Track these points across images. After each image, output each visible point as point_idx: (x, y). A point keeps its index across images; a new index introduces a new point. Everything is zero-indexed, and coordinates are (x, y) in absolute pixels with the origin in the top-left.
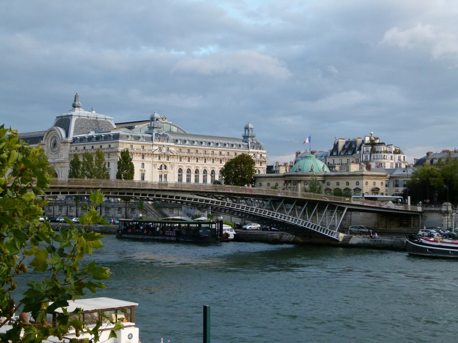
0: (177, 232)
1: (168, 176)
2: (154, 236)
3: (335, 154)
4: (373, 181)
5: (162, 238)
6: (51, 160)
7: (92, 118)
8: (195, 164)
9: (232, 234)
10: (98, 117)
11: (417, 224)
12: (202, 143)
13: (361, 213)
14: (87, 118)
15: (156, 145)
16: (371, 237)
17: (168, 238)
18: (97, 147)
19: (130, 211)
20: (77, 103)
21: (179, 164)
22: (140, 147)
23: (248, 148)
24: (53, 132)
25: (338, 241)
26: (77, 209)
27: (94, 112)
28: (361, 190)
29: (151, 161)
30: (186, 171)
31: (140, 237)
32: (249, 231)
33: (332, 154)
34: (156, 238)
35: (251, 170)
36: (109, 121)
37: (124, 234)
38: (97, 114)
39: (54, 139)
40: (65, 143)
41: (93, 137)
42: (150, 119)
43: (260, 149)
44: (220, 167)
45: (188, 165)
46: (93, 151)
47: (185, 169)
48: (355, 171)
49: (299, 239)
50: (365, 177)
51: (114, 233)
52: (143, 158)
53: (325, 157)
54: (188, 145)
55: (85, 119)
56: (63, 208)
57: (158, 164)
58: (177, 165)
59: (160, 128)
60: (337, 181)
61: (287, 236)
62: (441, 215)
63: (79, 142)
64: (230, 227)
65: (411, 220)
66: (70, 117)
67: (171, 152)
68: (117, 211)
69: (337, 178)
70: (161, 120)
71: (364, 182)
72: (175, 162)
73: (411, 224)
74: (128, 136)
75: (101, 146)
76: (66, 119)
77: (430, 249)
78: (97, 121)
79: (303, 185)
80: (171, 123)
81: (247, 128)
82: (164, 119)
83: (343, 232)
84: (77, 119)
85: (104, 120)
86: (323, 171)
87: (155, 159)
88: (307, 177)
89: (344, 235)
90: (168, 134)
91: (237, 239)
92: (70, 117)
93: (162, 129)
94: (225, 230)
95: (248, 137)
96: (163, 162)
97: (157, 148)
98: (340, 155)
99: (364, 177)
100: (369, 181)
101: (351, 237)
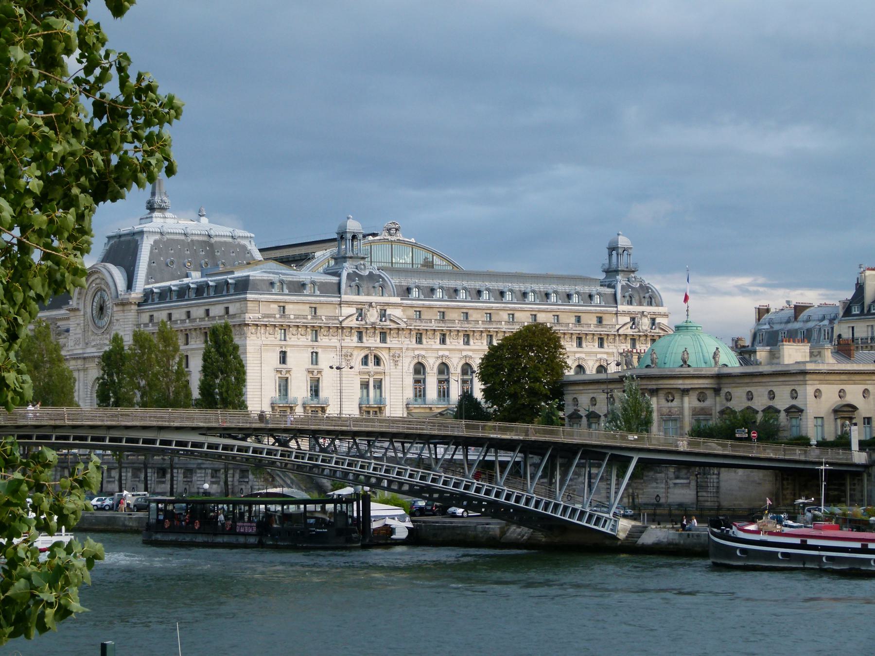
0: (260, 525)
1: (386, 385)
2: (215, 535)
3: (856, 311)
4: (837, 388)
5: (232, 539)
6: (94, 350)
7: (196, 238)
8: (461, 350)
10: (212, 233)
11: (858, 496)
12: (479, 292)
13: (740, 471)
14: (183, 237)
15: (349, 304)
16: (683, 526)
17: (242, 540)
18: (162, 316)
19: (237, 476)
20: (157, 199)
21: (417, 353)
22: (305, 310)
23: (616, 302)
24: (96, 276)
25: (614, 538)
26: (120, 476)
27: (204, 220)
28: (801, 411)
29: (338, 345)
30: (435, 370)
31: (188, 539)
32: (461, 520)
33: (848, 312)
34: (219, 539)
35: (555, 366)
36: (243, 242)
37: (157, 532)
38: (212, 226)
39: (99, 293)
40: (124, 304)
41: (189, 288)
42: (335, 236)
43: (650, 304)
45: (441, 353)
46: (151, 328)
47: (432, 365)
48: (797, 363)
49: (541, 537)
51: (136, 532)
53: (832, 321)
54: (439, 300)
55: (177, 241)
57: (355, 353)
58: (411, 353)
59: (363, 258)
60: (748, 389)
61: (516, 532)
63: (157, 300)
64: (402, 512)
65: (844, 485)
66: (137, 238)
69: (747, 380)
70: (385, 235)
71: (810, 389)
73: (845, 496)
74: (272, 284)
75: (170, 315)
76: (129, 242)
77: (743, 551)
78: (211, 245)
79: (696, 404)
80: (413, 240)
81: (613, 248)
82: (393, 231)
84: (155, 242)
85: (230, 240)
86: (716, 363)
87: (348, 339)
89: (633, 523)
90: (383, 274)
91: (415, 539)
92: (137, 238)
93: (367, 262)
95: (617, 272)
97: (628, 319)
98: (869, 313)
99: (808, 377)
100: (823, 388)
101: (646, 527)
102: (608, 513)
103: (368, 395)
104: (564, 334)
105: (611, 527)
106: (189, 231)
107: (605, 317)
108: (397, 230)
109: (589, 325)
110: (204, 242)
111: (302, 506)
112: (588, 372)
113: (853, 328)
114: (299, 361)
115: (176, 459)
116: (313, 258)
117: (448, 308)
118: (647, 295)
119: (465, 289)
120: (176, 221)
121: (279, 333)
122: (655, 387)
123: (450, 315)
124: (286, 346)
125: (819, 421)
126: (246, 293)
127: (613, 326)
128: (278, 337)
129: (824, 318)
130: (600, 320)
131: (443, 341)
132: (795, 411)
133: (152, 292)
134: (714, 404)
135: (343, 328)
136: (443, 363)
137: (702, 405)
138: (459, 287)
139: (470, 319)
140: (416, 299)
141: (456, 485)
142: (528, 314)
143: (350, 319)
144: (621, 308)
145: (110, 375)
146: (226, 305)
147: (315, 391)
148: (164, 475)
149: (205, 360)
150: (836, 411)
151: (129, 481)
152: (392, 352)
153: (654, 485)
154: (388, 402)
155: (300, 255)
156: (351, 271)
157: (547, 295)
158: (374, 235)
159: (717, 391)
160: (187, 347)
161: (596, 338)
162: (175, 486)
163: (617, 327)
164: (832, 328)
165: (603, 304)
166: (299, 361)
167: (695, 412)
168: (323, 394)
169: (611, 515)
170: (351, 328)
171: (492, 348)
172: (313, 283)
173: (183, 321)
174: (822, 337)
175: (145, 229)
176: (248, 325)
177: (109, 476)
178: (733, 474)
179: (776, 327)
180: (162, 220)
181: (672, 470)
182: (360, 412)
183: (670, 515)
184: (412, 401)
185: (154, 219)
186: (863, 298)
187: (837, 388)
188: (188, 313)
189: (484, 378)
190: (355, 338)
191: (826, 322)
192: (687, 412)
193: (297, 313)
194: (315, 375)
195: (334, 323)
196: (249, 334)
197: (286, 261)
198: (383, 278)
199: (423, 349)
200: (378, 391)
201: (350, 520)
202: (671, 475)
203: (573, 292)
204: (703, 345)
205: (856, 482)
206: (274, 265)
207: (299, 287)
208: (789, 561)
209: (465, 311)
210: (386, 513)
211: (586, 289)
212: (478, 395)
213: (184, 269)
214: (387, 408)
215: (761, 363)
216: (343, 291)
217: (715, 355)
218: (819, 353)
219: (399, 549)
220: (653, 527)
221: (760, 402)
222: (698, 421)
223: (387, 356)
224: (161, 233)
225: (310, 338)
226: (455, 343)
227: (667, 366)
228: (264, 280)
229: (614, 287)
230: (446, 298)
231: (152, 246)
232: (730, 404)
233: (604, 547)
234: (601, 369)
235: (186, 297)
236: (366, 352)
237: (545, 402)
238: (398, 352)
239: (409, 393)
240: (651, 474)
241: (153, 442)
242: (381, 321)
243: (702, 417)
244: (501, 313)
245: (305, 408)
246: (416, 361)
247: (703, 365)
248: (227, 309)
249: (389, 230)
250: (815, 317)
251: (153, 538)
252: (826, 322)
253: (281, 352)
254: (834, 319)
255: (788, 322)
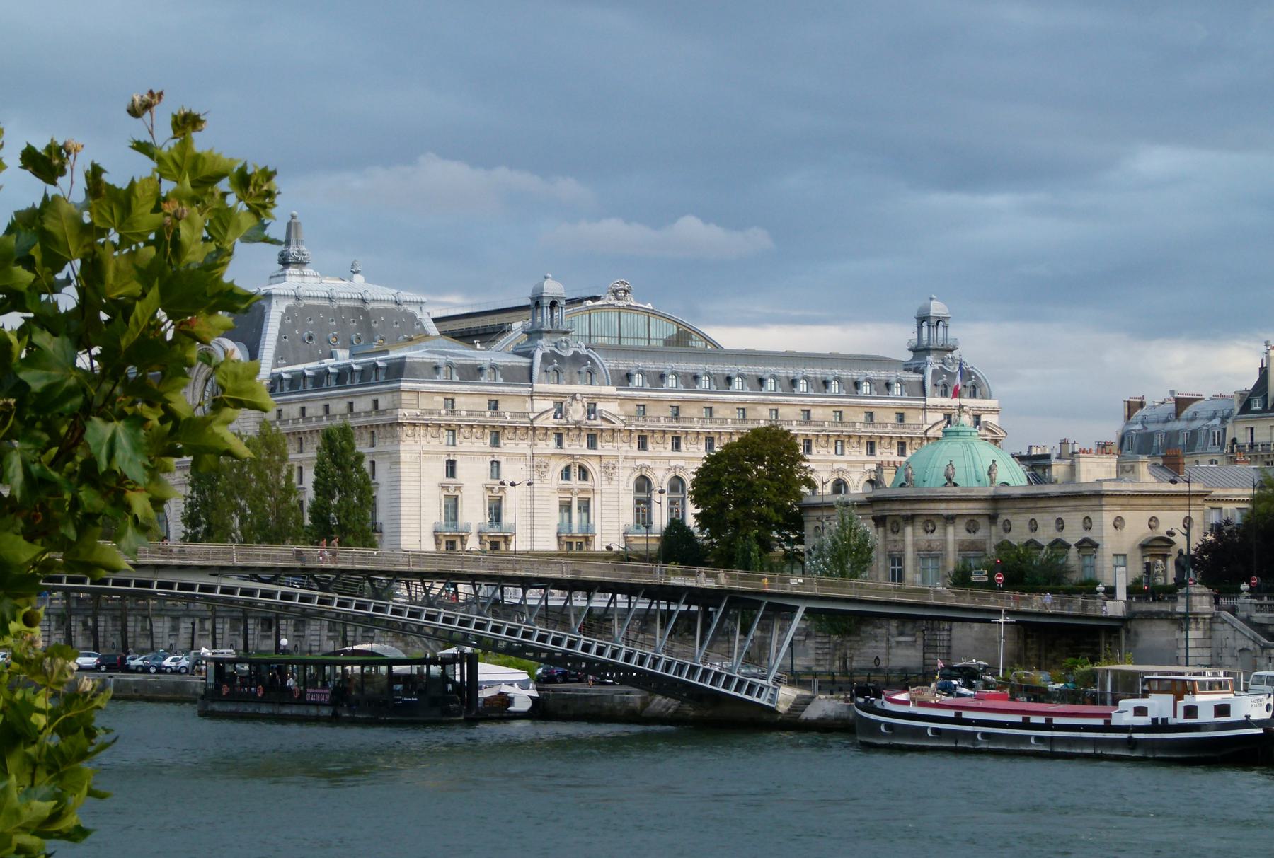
1: (595, 506)
3: (1256, 406)
4: (1146, 515)
9: (522, 699)
10: (367, 296)
12: (729, 380)
13: (976, 626)
14: (327, 303)
15: (545, 395)
17: (313, 711)
20: (293, 250)
21: (639, 462)
25: (773, 711)
26: (214, 628)
27: (359, 279)
28: (1096, 546)
29: (528, 451)
31: (250, 710)
33: (1246, 408)
34: (287, 710)
36: (410, 309)
37: (213, 701)
38: (370, 286)
41: (327, 373)
42: (529, 302)
43: (973, 395)
44: (868, 467)
45: (673, 463)
47: (661, 478)
49: (690, 711)
50: (1114, 500)
51: (193, 702)
52: (495, 443)
53: (1224, 420)
54: (671, 391)
55: (318, 308)
56: (182, 625)
57: (552, 463)
58: (631, 464)
60: (1031, 516)
61: (660, 703)
62: (1174, 627)
63: (286, 389)
64: (525, 677)
65: (1098, 644)
66: (264, 303)
67: (603, 418)
68: (325, 632)
69: (1030, 505)
70: (609, 299)
71: (1108, 518)
72: (622, 454)
74: (436, 368)
77: (888, 726)
78: (366, 314)
79: (964, 535)
80: (649, 306)
82: (621, 294)
83: (791, 683)
84: (288, 309)
85: (393, 306)
86: (992, 481)
87: (541, 444)
88: (932, 506)
91: (539, 711)
92: (264, 303)
94: (491, 684)
96: (572, 456)
97: (940, 417)
99: (1105, 500)
100: (1127, 515)
101: (812, 698)
102: (765, 678)
103: (570, 521)
104: (849, 437)
105: (768, 696)
106: (335, 294)
107: (908, 413)
108: (626, 292)
109: (885, 425)
110: (357, 309)
111: (339, 669)
112: (852, 490)
113: (1252, 429)
114: (473, 475)
115: (191, 606)
116: (510, 330)
117: (684, 401)
118: (969, 383)
119: (708, 374)
120: (318, 280)
121: (445, 436)
122: (909, 513)
123: (686, 411)
124: (455, 453)
125: (1121, 560)
126: (399, 381)
127: (919, 426)
128: (445, 440)
129: (1213, 418)
130: (901, 418)
131: (677, 447)
132: (1088, 546)
133: (280, 378)
134: (989, 536)
135: (535, 429)
136: (677, 477)
137: (972, 537)
138: (700, 373)
139: (715, 416)
140: (639, 389)
141: (557, 641)
142: (798, 409)
143: (545, 416)
144: (931, 401)
145: (201, 492)
146: (375, 397)
147: (496, 513)
148: (270, 629)
149: (317, 474)
150: (1143, 547)
151: (226, 636)
152: (604, 461)
153: (873, 643)
154: (597, 530)
155: (493, 327)
156: (547, 350)
157: (826, 383)
158: (596, 298)
159: (993, 518)
160: (301, 456)
161: (895, 442)
162: (250, 642)
163: (926, 427)
164: (1225, 430)
165: (905, 395)
166: (473, 475)
167: (963, 547)
168: (507, 519)
169: (770, 681)
170: (546, 428)
171: (710, 459)
172: (494, 368)
173: (319, 418)
174: (1211, 442)
175: (274, 292)
176: (402, 424)
177: (203, 629)
178: (968, 630)
179: (1151, 428)
180: (299, 279)
181: (894, 624)
182: (559, 544)
183: (833, 682)
184: (633, 529)
185: (288, 278)
186: (1266, 389)
187: (1146, 515)
188: (327, 407)
189: (697, 501)
190: (552, 442)
191: (1217, 421)
192: (951, 547)
193: (472, 408)
194: (496, 493)
195: (524, 422)
196: (403, 437)
197: (465, 337)
198: (593, 362)
199: (647, 458)
200: (585, 515)
201: (450, 687)
202: (893, 630)
203: (862, 379)
204: (975, 454)
205: (1112, 640)
206: (446, 342)
207: (473, 373)
208: (940, 739)
209: (708, 405)
210: (495, 676)
211: (883, 375)
212: (691, 522)
213: (327, 346)
214: (597, 539)
215: (1056, 481)
216: (535, 377)
217: (991, 470)
218: (1133, 467)
219: (519, 724)
220: (823, 697)
221: (1046, 535)
222: (965, 558)
223: (597, 468)
224: (297, 298)
225: (488, 442)
226: (660, 449)
227: (927, 485)
228: (425, 363)
229: (922, 372)
230: (681, 387)
231: (283, 315)
232: (1008, 537)
233: (754, 723)
234: (839, 486)
235: (324, 386)
236: (568, 461)
237: (779, 533)
238: (612, 461)
239: (629, 518)
240: (869, 629)
241: (149, 584)
242: (589, 418)
243: (971, 553)
244: (759, 408)
245: (481, 537)
246: (638, 474)
247: (975, 484)
248: (376, 402)
249: (615, 292)
250: (1203, 414)
251: (209, 708)
252: (1217, 421)
253: (492, 462)
254: (1228, 417)
255: (1167, 421)
